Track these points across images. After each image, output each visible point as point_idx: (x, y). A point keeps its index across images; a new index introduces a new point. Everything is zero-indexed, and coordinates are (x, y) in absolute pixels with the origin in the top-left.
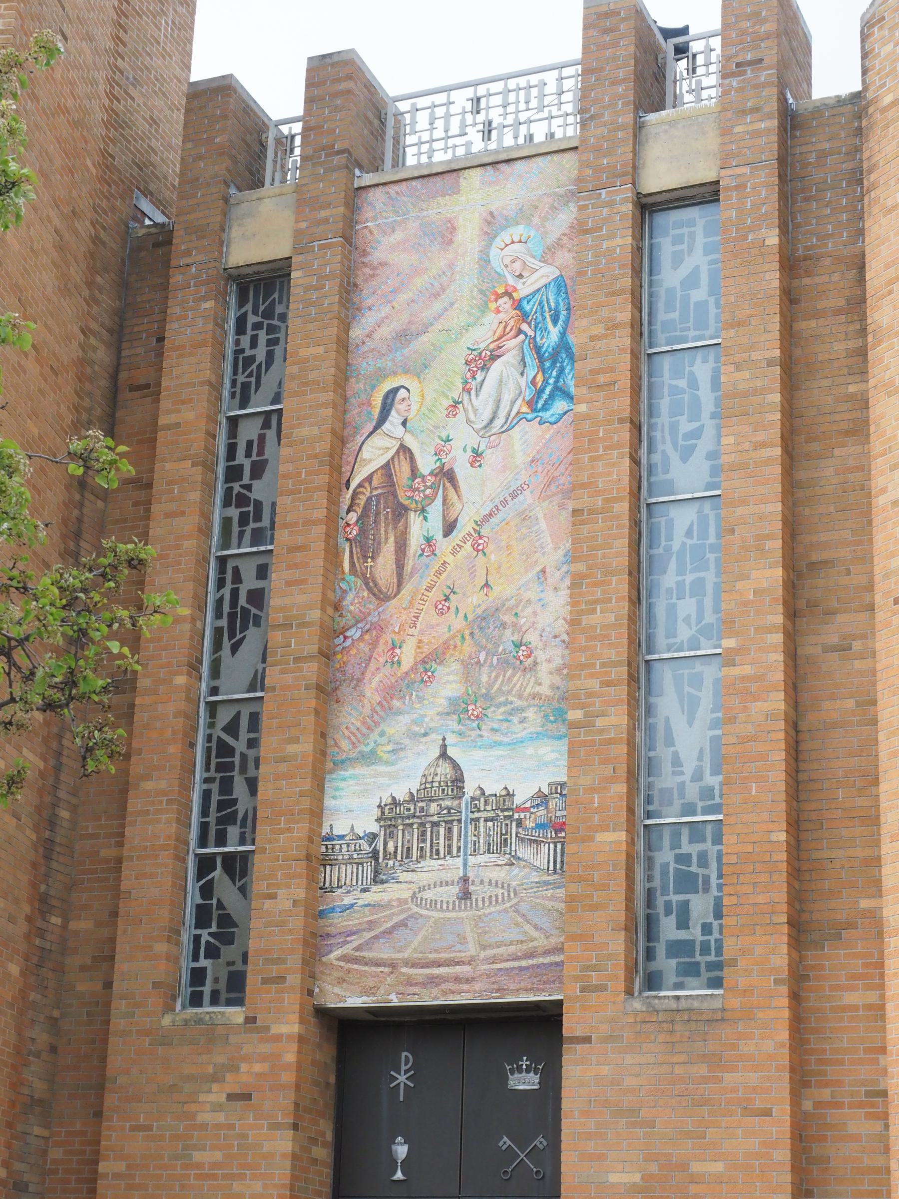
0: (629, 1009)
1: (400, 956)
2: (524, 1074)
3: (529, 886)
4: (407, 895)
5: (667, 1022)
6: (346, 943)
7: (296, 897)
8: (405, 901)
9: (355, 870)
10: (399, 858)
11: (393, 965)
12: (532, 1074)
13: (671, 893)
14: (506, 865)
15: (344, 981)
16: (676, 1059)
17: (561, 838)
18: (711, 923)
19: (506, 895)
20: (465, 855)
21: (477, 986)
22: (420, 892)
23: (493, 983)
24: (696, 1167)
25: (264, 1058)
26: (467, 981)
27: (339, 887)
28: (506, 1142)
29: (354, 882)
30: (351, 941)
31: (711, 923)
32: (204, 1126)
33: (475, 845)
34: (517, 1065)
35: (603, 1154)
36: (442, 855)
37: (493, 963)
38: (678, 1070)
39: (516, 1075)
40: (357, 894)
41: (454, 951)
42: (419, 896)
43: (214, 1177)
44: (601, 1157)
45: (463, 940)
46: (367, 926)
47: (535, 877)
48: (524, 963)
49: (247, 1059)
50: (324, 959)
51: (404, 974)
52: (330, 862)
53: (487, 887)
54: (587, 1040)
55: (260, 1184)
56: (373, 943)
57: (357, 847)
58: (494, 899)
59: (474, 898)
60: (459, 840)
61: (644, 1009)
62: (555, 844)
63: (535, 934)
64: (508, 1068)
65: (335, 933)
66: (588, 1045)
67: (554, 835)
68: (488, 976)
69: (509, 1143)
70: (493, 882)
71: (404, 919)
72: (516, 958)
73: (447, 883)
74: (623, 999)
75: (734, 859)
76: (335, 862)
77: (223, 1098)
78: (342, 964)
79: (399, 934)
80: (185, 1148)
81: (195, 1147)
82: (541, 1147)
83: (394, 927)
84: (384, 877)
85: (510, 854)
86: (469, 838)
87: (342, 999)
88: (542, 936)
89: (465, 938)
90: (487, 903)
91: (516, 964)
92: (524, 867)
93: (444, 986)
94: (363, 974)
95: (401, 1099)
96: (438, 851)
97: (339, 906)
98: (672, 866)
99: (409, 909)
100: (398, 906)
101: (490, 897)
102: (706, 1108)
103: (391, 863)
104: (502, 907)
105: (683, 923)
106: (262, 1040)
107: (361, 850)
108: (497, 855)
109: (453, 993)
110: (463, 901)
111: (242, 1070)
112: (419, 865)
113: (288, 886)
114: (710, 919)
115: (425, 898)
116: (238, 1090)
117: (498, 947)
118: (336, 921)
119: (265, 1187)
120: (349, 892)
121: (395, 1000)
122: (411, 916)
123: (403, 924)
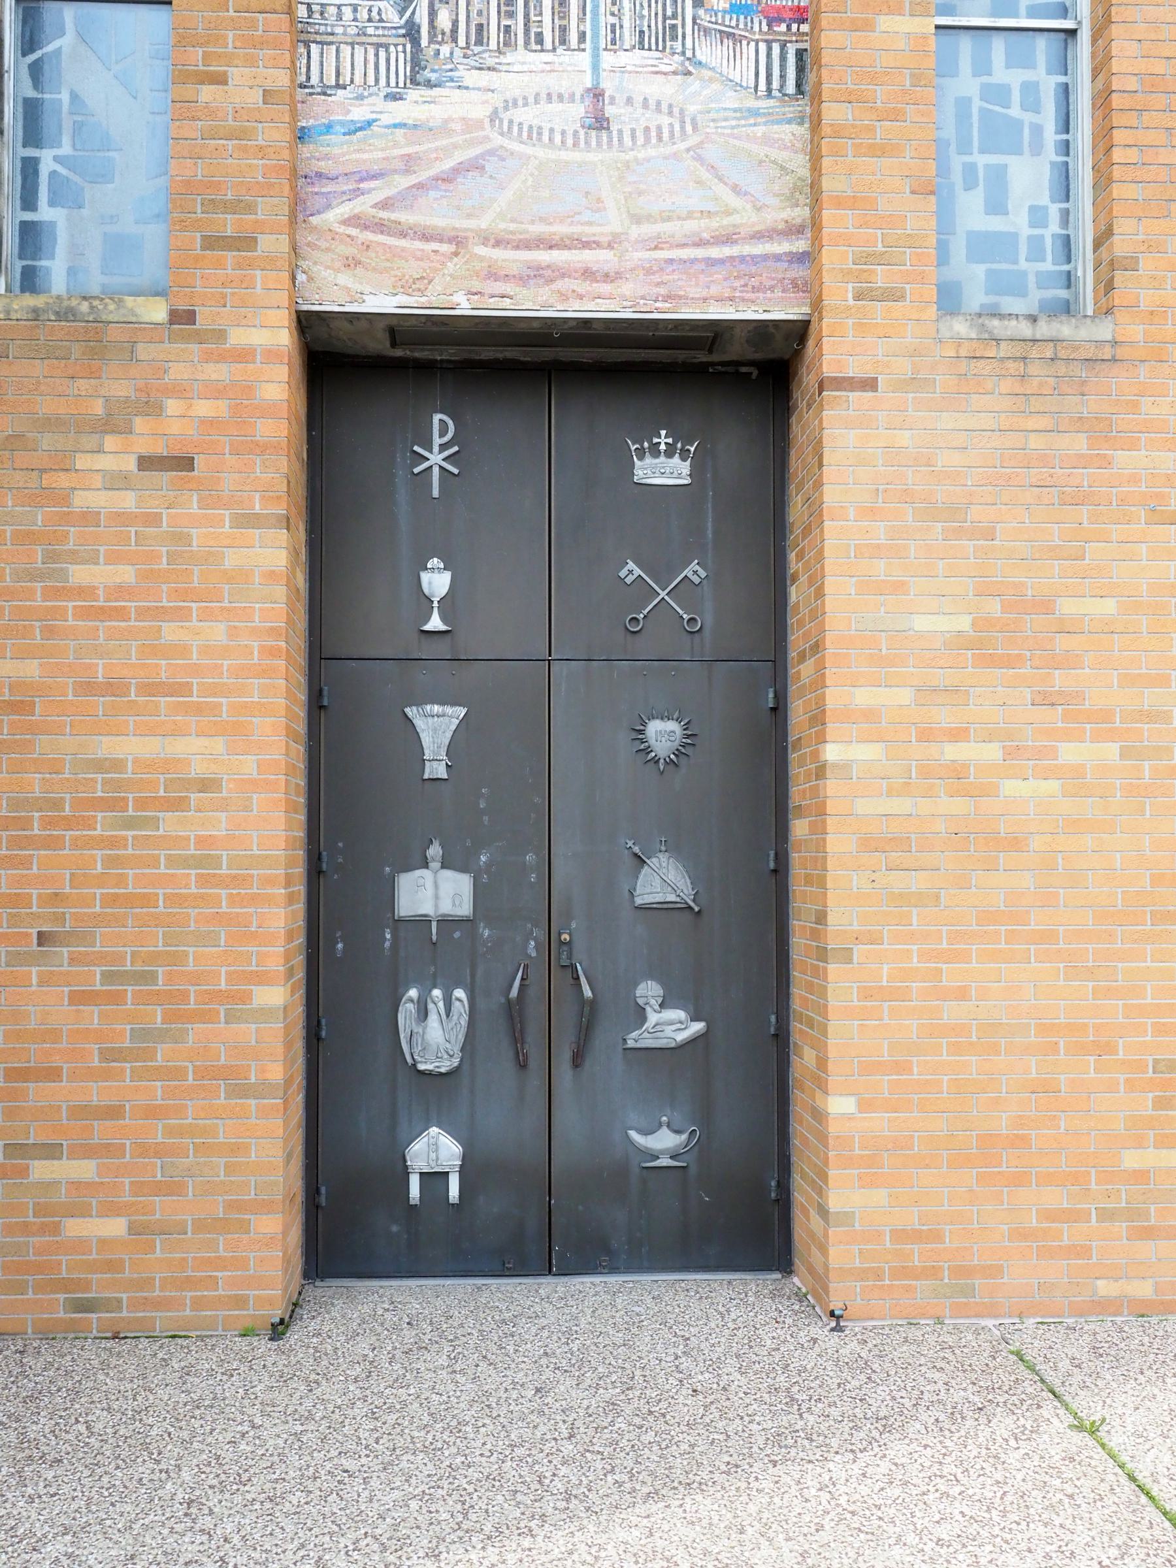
0: (945, 333)
1: (472, 224)
2: (662, 459)
3: (722, 114)
4: (481, 112)
5: (1015, 359)
6: (357, 193)
7: (269, 85)
8: (479, 124)
9: (371, 58)
10: (462, 41)
11: (458, 241)
12: (676, 459)
13: (975, 150)
14: (675, 73)
15: (358, 263)
16: (1031, 424)
17: (780, 33)
18: (1046, 208)
19: (677, 128)
20: (596, 49)
21: (627, 288)
22: (506, 108)
23: (658, 284)
24: (1067, 607)
25: (216, 391)
26: (607, 278)
27: (338, 86)
28: (632, 570)
29: (371, 80)
30: (369, 191)
31: (1046, 208)
32: (89, 518)
33: (613, 31)
34: (650, 442)
35: (903, 583)
36: (548, 44)
37: (656, 248)
38: (1035, 442)
39: (649, 460)
40: (378, 102)
41: (579, 223)
42: (506, 116)
43: (120, 614)
44: (899, 588)
45: (598, 205)
46: (400, 165)
47: (731, 100)
48: (715, 252)
49: (179, 391)
50: (314, 220)
51: (481, 259)
52: (318, 38)
53: (640, 111)
54: (870, 384)
55: (222, 627)
56: (415, 197)
57: (374, 14)
58: (653, 134)
59: (614, 128)
60: (581, 20)
61: (974, 336)
62: (769, 43)
63: (734, 201)
64: (633, 448)
65: (333, 173)
66: (870, 394)
67: (765, 28)
68: (649, 272)
69: (638, 571)
70: (652, 103)
71: (477, 157)
72: (700, 243)
73: (560, 97)
74: (934, 317)
75: (1132, 84)
76: (330, 39)
77: (131, 464)
78: (353, 232)
79: (468, 183)
80: (51, 557)
81: (75, 557)
82: (696, 580)
83: (457, 170)
84: (433, 77)
85: (683, 53)
86: (602, 19)
87: (360, 297)
88: (749, 206)
89: (599, 200)
90: (641, 140)
91: (700, 253)
92: (711, 80)
93: (559, 285)
94: (396, 254)
95: (436, 493)
96: (540, 39)
97: (342, 123)
98: (977, 104)
99: (487, 138)
100: (464, 132)
101: (647, 129)
102: (1084, 509)
103: (445, 50)
104: (669, 150)
105: (996, 205)
106: (208, 358)
107: (381, 20)
108: (658, 54)
109: (581, 297)
110: (593, 133)
111: (170, 412)
112: (502, 59)
113: (251, 62)
114: (1044, 199)
115: (517, 120)
116: (161, 449)
117: (664, 220)
118: (336, 151)
119: (233, 633)
120: (361, 97)
121: (465, 304)
122: (491, 152)
123: (475, 166)
